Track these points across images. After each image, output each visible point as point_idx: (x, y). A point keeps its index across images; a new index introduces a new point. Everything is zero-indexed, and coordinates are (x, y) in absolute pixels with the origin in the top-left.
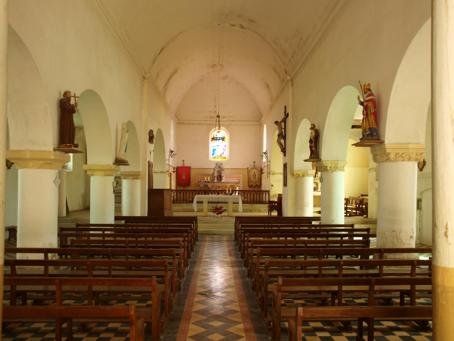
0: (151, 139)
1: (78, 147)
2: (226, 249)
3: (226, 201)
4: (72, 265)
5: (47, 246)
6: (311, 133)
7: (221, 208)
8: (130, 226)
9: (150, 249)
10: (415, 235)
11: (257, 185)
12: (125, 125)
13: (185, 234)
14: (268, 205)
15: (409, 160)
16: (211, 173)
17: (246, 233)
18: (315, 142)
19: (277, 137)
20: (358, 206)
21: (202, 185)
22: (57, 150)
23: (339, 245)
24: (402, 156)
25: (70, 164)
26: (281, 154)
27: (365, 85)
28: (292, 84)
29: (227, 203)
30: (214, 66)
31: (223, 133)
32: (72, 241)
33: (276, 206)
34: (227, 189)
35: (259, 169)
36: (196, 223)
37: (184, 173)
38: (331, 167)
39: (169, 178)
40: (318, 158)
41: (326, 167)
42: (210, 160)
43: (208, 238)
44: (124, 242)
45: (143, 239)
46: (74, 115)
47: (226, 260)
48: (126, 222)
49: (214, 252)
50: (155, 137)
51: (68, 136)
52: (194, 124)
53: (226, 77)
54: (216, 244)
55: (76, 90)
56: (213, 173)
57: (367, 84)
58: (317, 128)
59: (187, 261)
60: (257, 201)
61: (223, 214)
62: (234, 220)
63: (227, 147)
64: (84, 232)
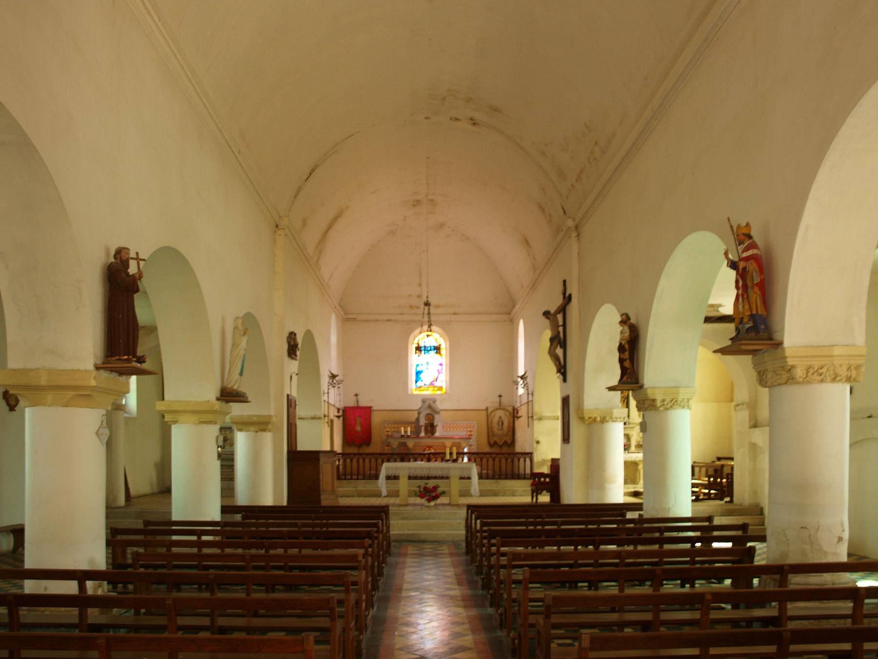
0: (292, 350)
1: (144, 362)
2: (451, 572)
3: (445, 473)
4: (136, 605)
5: (84, 566)
6: (622, 332)
7: (435, 488)
8: (253, 525)
9: (296, 572)
10: (846, 535)
11: (505, 442)
12: (240, 321)
13: (368, 541)
14: (530, 481)
15: (834, 380)
16: (413, 419)
17: (494, 538)
18: (630, 351)
19: (547, 344)
20: (716, 479)
21: (395, 444)
22: (101, 368)
23: (688, 559)
24: (820, 371)
25: (131, 400)
26: (556, 378)
27: (739, 226)
28: (578, 235)
29: (448, 478)
30: (417, 203)
31: (435, 338)
32: (136, 555)
33: (547, 483)
34: (448, 451)
35: (511, 409)
36: (387, 518)
37: (359, 420)
38: (663, 401)
39: (327, 430)
40: (637, 383)
41: (654, 400)
42: (410, 392)
43: (411, 550)
44: (241, 557)
45: (280, 551)
46: (137, 298)
47: (452, 593)
48: (244, 518)
49: (426, 577)
50: (300, 346)
51: (124, 341)
52: (376, 320)
53: (442, 225)
54: (429, 561)
55: (142, 246)
56: (418, 420)
57: (744, 224)
58: (633, 321)
59: (373, 596)
60: (506, 475)
61: (439, 501)
62: (463, 512)
63: (444, 367)
64: (159, 538)
